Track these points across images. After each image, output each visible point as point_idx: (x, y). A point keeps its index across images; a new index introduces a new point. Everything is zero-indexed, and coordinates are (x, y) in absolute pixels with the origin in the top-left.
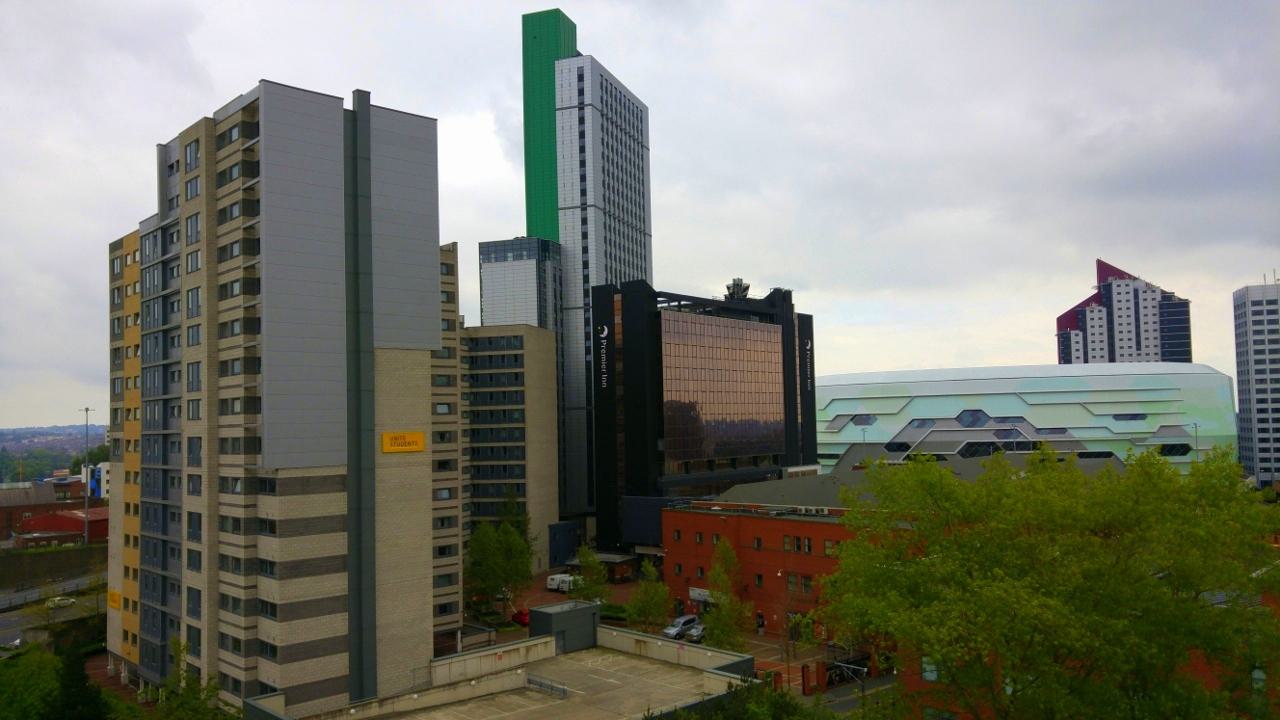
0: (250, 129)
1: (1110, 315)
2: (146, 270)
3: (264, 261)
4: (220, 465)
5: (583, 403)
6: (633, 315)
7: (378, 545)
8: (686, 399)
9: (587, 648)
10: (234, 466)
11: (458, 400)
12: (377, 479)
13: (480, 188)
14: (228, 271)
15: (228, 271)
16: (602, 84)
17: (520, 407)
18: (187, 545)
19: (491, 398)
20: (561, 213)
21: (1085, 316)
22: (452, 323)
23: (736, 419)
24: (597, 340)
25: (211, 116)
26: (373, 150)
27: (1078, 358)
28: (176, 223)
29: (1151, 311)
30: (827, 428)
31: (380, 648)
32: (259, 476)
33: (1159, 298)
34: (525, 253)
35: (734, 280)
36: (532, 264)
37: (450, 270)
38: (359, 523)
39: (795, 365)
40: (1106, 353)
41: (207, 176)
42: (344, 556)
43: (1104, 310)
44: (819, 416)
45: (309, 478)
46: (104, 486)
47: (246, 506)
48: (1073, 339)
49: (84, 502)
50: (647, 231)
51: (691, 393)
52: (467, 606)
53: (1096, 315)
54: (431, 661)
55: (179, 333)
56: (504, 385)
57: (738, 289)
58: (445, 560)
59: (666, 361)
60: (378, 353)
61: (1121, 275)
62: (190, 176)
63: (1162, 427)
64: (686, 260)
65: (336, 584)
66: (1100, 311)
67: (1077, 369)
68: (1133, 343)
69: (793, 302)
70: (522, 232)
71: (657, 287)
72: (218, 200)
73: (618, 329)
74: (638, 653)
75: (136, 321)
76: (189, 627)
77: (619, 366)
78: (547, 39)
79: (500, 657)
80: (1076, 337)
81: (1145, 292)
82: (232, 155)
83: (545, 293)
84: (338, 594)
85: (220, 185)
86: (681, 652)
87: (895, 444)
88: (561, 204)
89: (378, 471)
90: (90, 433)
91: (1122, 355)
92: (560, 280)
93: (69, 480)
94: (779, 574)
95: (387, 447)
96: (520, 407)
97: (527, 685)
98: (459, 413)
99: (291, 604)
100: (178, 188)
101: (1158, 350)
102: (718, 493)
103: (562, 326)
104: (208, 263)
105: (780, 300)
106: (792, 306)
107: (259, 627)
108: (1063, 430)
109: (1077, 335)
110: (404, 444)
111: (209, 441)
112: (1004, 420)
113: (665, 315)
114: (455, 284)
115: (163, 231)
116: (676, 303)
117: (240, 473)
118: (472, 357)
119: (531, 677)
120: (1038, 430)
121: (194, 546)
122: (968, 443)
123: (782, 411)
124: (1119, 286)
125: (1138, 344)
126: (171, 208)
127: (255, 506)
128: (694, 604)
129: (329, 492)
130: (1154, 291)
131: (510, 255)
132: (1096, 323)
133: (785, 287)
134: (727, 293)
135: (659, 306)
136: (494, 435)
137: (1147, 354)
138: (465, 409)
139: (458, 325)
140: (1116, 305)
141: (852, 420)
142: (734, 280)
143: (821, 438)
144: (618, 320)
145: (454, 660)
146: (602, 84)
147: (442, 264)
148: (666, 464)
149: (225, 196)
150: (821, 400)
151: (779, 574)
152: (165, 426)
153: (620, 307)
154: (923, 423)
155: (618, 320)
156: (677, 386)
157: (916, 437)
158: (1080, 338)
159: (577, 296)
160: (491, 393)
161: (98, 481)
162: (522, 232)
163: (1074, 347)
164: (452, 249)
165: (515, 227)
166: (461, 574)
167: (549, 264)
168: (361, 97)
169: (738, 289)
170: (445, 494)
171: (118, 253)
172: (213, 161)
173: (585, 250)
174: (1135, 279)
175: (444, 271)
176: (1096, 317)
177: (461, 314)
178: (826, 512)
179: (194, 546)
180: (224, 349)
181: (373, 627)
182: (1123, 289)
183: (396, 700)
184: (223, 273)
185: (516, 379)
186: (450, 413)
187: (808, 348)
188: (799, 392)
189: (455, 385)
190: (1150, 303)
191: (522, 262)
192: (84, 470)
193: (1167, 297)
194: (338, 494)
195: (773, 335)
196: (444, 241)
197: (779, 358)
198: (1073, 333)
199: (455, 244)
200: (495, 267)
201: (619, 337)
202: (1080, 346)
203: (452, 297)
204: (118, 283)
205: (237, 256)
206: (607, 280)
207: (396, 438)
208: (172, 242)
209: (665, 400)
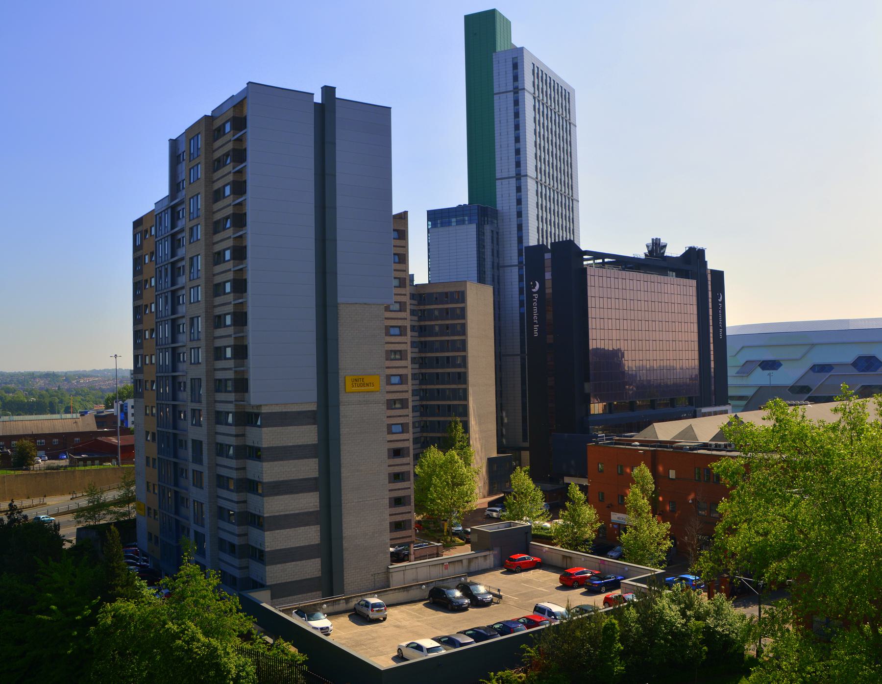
0: (240, 123)
2: (158, 245)
3: (249, 268)
4: (216, 401)
5: (518, 351)
6: (564, 269)
7: (343, 470)
8: (609, 346)
10: (227, 402)
11: (408, 347)
12: (342, 414)
13: (428, 173)
14: (222, 241)
15: (222, 241)
16: (533, 71)
17: (462, 354)
18: (192, 466)
19: (437, 363)
20: (498, 183)
22: (405, 280)
23: (655, 365)
24: (530, 294)
25: (209, 114)
26: (341, 137)
28: (182, 202)
30: (738, 373)
31: (346, 555)
32: (247, 410)
34: (466, 218)
36: (472, 228)
37: (402, 235)
38: (327, 451)
39: (708, 298)
41: (206, 163)
42: (315, 479)
44: (730, 362)
46: (131, 419)
49: (116, 431)
50: (572, 121)
51: (614, 342)
52: (413, 328)
55: (183, 206)
56: (449, 399)
57: (656, 247)
58: (398, 461)
59: (592, 313)
60: (341, 307)
62: (193, 163)
64: (606, 227)
65: (309, 468)
70: (465, 201)
71: (583, 247)
72: (214, 182)
73: (549, 284)
75: (151, 335)
76: (196, 533)
77: (549, 316)
78: (482, 30)
82: (224, 144)
83: (483, 240)
85: (216, 232)
88: (498, 175)
89: (342, 408)
90: (119, 375)
92: (497, 238)
93: (105, 413)
96: (462, 354)
98: (409, 359)
100: (184, 174)
102: (638, 431)
103: (498, 244)
104: (206, 234)
105: (695, 256)
106: (705, 263)
111: (207, 381)
113: (590, 271)
114: (406, 247)
115: (171, 208)
116: (601, 261)
118: (421, 342)
121: (197, 467)
123: (697, 357)
126: (178, 190)
127: (243, 435)
128: (615, 526)
129: (302, 425)
131: (454, 220)
133: (698, 245)
134: (646, 251)
135: (585, 263)
136: (441, 395)
138: (415, 355)
139: (408, 282)
143: (731, 381)
144: (548, 276)
146: (533, 71)
147: (394, 230)
148: (592, 405)
149: (218, 179)
150: (731, 349)
152: (174, 369)
153: (550, 265)
155: (548, 276)
156: (601, 336)
159: (512, 255)
160: (437, 358)
161: (126, 414)
162: (465, 201)
164: (403, 216)
165: (458, 195)
166: (412, 497)
167: (488, 229)
168: (329, 91)
169: (656, 247)
170: (395, 380)
171: (140, 229)
172: (209, 149)
175: (397, 260)
177: (410, 273)
179: (197, 467)
180: (218, 274)
181: (341, 538)
184: (217, 243)
185: (459, 378)
186: (400, 335)
187: (720, 300)
188: (710, 306)
189: (406, 335)
191: (464, 227)
192: (115, 404)
194: (309, 426)
195: (690, 286)
196: (396, 211)
197: (694, 309)
199: (406, 213)
200: (442, 231)
201: (549, 291)
203: (402, 258)
204: (139, 253)
205: (229, 293)
206: (538, 240)
207: (356, 380)
208: (179, 218)
209: (591, 348)
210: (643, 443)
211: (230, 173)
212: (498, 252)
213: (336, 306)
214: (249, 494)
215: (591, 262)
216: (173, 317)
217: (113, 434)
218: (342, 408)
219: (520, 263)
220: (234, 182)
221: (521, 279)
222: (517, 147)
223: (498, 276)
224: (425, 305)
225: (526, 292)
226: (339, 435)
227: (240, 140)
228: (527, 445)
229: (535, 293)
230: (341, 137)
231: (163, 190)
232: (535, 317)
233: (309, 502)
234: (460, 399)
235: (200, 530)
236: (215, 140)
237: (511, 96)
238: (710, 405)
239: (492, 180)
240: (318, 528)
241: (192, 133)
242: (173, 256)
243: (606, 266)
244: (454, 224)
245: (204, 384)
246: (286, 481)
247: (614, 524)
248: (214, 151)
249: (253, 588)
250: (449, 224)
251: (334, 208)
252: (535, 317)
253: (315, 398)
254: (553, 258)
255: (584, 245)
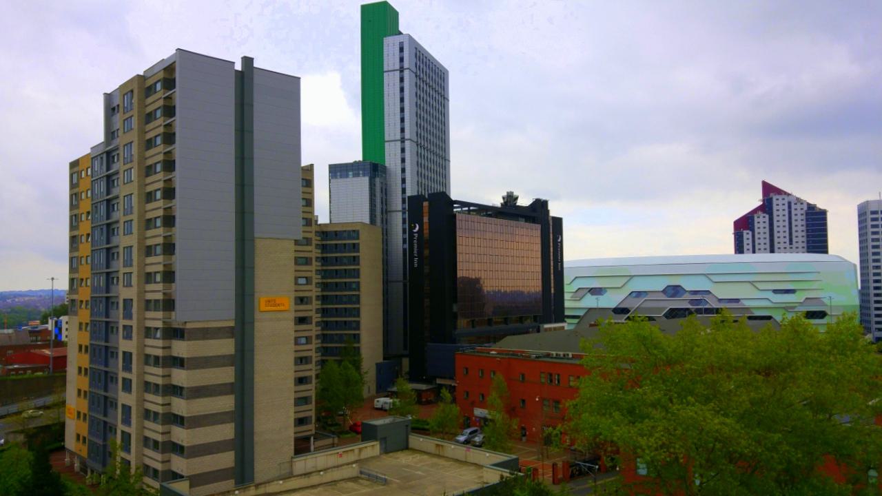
0: (169, 83)
1: (771, 220)
6: (437, 216)
9: (402, 450)
10: (156, 319)
11: (313, 275)
13: (330, 126)
18: (122, 374)
19: (337, 274)
20: (386, 144)
21: (753, 220)
22: (310, 221)
23: (508, 290)
24: (411, 234)
25: (142, 74)
27: (748, 250)
28: (117, 149)
29: (799, 217)
30: (572, 297)
33: (805, 208)
34: (361, 172)
35: (508, 193)
36: (365, 181)
40: (768, 246)
42: (232, 384)
43: (767, 216)
44: (567, 289)
45: (208, 328)
46: (64, 333)
47: (163, 348)
48: (745, 236)
49: (50, 344)
52: (318, 337)
53: (761, 220)
54: (292, 458)
56: (345, 265)
57: (510, 199)
58: (303, 387)
61: (779, 192)
62: (127, 115)
63: (807, 299)
64: (474, 179)
66: (764, 217)
67: (747, 257)
68: (787, 240)
69: (549, 208)
73: (426, 226)
74: (438, 453)
75: (87, 217)
76: (123, 432)
77: (426, 252)
79: (341, 456)
80: (747, 235)
81: (796, 204)
82: (156, 102)
84: (227, 410)
85: (148, 122)
86: (468, 453)
87: (620, 308)
91: (779, 248)
92: (385, 191)
93: (39, 328)
94: (537, 399)
95: (263, 308)
97: (360, 475)
99: (194, 416)
101: (805, 245)
104: (139, 176)
105: (540, 207)
107: (172, 433)
108: (737, 300)
109: (748, 234)
110: (275, 305)
111: (138, 301)
112: (696, 292)
113: (459, 217)
114: (312, 193)
115: (107, 154)
116: (467, 209)
117: (159, 324)
119: (363, 470)
120: (720, 300)
122: (671, 309)
124: (777, 199)
125: (791, 240)
130: (802, 204)
131: (351, 173)
132: (762, 225)
133: (543, 198)
135: (455, 210)
136: (338, 299)
137: (797, 248)
140: (775, 213)
141: (589, 291)
142: (508, 193)
143: (567, 304)
144: (426, 219)
145: (308, 457)
146: (416, 54)
148: (459, 321)
151: (537, 399)
154: (639, 294)
155: (426, 219)
157: (633, 304)
158: (750, 236)
159: (397, 203)
161: (60, 329)
162: (360, 158)
163: (745, 242)
164: (310, 169)
165: (355, 154)
167: (378, 180)
168: (248, 61)
169: (510, 199)
171: (76, 169)
172: (142, 105)
173: (403, 170)
174: (789, 195)
175: (305, 184)
176: (761, 221)
177: (316, 214)
178: (570, 356)
179: (127, 375)
180: (150, 238)
181: (252, 434)
182: (780, 202)
183: (267, 485)
184: (148, 292)
185: (354, 260)
187: (559, 240)
190: (799, 212)
191: (359, 179)
192: (50, 321)
193: (811, 208)
195: (535, 231)
198: (745, 232)
199: (312, 166)
200: (340, 182)
201: (426, 232)
202: (750, 241)
203: (309, 202)
204: (76, 190)
205: (159, 200)
207: (269, 301)
208: (113, 162)
209: (458, 276)
210: (500, 353)
211: (161, 125)
212: (387, 220)
213: (253, 240)
214: (172, 397)
215: (459, 209)
216: (108, 246)
217: (47, 346)
218: (257, 324)
219: (404, 209)
220: (164, 133)
221: (404, 222)
222: (404, 187)
223: (387, 229)
224: (327, 241)
225: (410, 238)
226: (253, 346)
227: (169, 98)
228: (407, 352)
229: (416, 233)
230: (255, 100)
231: (99, 137)
232: (415, 252)
233: (226, 403)
234: (354, 316)
235: (126, 429)
236: (147, 97)
237: (399, 144)
238: (550, 322)
239: (382, 141)
240: (233, 425)
241: (127, 89)
242: (108, 194)
243: (472, 213)
244: (351, 176)
245: (135, 304)
246: (207, 386)
247: (476, 417)
248: (146, 106)
249: (173, 479)
250: (347, 176)
251: (252, 159)
252: (415, 252)
253: (232, 314)
254: (430, 206)
255: (454, 196)
